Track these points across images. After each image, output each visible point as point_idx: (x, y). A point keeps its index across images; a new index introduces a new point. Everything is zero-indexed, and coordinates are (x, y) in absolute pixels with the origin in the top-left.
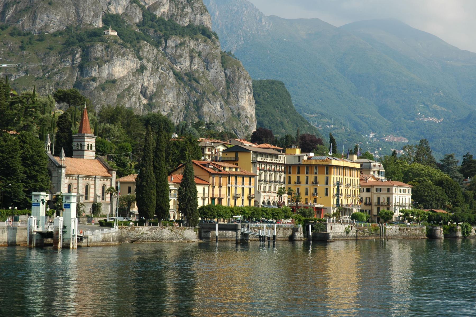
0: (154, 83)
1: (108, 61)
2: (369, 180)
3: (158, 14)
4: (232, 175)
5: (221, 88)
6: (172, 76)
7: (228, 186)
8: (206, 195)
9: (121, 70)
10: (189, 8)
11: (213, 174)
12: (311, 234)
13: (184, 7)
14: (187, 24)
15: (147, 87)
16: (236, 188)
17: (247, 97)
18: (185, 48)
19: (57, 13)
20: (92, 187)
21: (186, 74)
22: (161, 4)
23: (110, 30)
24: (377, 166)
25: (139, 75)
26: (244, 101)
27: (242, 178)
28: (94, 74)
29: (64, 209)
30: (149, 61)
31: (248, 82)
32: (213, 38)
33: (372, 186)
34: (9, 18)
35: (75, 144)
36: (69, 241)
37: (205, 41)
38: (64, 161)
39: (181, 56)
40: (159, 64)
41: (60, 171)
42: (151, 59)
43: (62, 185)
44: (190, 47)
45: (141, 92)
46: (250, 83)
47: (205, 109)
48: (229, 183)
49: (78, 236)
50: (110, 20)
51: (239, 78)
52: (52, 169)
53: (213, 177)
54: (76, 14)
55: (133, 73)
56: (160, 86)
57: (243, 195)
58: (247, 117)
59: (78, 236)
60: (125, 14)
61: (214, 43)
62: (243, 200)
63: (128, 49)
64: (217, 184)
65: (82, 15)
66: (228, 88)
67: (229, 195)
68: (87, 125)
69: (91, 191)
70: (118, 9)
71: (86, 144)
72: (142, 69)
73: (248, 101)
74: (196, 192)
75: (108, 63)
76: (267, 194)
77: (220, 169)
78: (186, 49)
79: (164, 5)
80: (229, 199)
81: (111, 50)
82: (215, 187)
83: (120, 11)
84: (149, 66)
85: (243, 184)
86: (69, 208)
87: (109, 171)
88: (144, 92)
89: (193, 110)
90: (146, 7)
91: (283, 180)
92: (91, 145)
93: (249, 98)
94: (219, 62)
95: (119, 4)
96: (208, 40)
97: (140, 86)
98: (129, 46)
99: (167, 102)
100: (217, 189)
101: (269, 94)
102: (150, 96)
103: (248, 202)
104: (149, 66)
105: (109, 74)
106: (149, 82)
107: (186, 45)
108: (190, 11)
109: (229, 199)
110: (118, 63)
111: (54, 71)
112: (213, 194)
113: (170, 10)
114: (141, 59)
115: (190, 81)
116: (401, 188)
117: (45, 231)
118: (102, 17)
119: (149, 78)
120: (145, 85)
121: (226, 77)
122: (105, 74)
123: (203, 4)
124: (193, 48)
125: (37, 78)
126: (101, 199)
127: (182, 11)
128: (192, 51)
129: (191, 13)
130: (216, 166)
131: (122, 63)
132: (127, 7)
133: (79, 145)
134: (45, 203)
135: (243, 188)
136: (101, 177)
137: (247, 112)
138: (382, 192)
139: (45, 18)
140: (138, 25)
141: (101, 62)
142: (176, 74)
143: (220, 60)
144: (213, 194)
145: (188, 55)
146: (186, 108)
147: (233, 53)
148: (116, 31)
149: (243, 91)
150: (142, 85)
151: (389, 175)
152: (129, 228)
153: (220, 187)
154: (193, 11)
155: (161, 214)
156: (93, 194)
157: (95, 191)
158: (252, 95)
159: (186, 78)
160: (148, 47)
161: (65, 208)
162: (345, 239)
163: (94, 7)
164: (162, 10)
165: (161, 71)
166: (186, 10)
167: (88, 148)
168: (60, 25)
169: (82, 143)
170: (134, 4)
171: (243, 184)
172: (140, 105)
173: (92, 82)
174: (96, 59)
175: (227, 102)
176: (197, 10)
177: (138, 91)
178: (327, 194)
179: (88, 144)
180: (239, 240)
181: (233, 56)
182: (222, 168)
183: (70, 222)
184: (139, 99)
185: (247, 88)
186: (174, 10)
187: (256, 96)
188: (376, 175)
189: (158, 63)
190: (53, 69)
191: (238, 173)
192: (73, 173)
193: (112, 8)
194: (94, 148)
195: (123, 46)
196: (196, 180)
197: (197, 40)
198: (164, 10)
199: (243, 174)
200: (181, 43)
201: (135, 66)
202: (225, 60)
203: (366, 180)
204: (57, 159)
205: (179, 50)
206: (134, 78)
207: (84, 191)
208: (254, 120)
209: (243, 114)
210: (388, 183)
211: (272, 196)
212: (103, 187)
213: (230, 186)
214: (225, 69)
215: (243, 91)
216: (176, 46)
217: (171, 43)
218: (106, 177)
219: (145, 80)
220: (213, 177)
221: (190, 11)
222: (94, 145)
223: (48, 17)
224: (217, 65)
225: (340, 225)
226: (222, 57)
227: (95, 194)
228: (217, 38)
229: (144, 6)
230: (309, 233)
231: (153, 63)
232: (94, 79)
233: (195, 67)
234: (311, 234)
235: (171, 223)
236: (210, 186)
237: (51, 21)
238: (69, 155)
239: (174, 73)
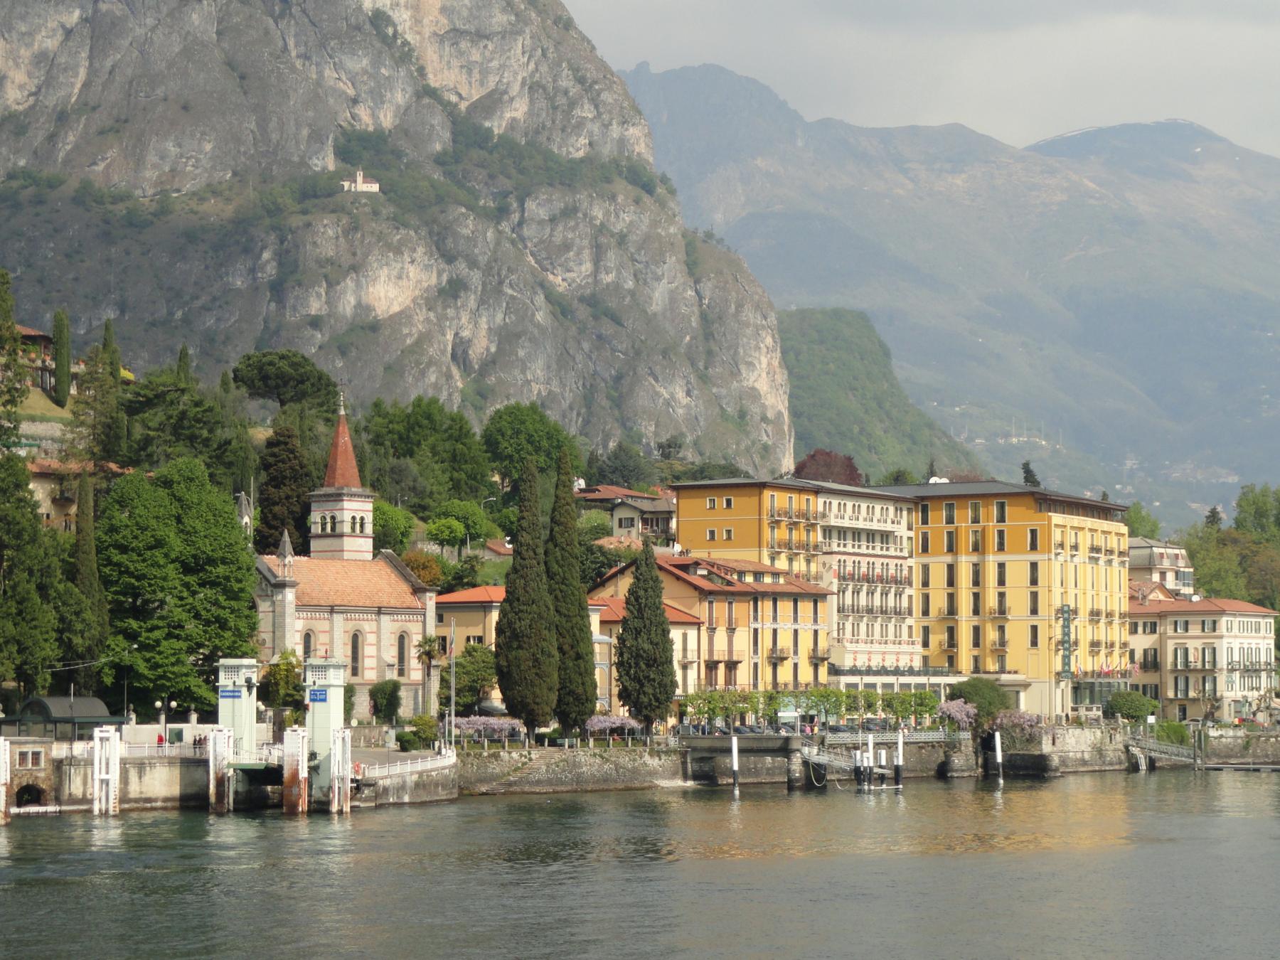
0: (490, 328)
1: (355, 268)
2: (1151, 597)
3: (496, 126)
4: (764, 595)
5: (688, 338)
6: (543, 305)
7: (753, 626)
8: (692, 656)
9: (392, 292)
10: (586, 107)
11: (711, 593)
12: (999, 759)
13: (572, 104)
14: (581, 154)
15: (470, 341)
16: (775, 631)
17: (764, 360)
18: (577, 224)
19: (203, 133)
20: (371, 638)
21: (582, 299)
22: (506, 97)
23: (360, 179)
24: (1172, 557)
25: (445, 308)
26: (756, 373)
27: (812, 604)
28: (315, 306)
29: (311, 705)
30: (473, 264)
31: (766, 318)
32: (660, 190)
33: (1162, 616)
34: (67, 155)
35: (315, 517)
36: (327, 795)
37: (637, 202)
38: (286, 565)
39: (567, 247)
40: (504, 273)
42: (480, 258)
43: (288, 635)
44: (593, 218)
45: (454, 357)
46: (772, 319)
47: (641, 399)
48: (756, 619)
49: (352, 781)
50: (360, 149)
51: (740, 306)
53: (711, 603)
54: (259, 137)
55: (427, 299)
56: (507, 337)
57: (796, 652)
58: (764, 419)
59: (352, 781)
60: (402, 129)
61: (662, 204)
62: (796, 665)
63: (412, 233)
64: (721, 622)
65: (275, 137)
66: (708, 336)
67: (756, 652)
68: (346, 465)
69: (368, 651)
70: (382, 116)
71: (347, 516)
72: (452, 291)
73: (768, 373)
74: (671, 642)
75: (354, 275)
76: (862, 647)
77: (728, 577)
78: (581, 225)
79: (512, 99)
80: (756, 665)
81: (363, 236)
82: (717, 632)
83: (387, 120)
84: (475, 278)
85: (796, 620)
87: (417, 591)
88: (460, 355)
89: (605, 403)
90: (463, 106)
91: (905, 604)
92: (362, 519)
93: (769, 364)
94: (678, 261)
95: (383, 103)
96: (646, 199)
97: (450, 337)
98: (414, 221)
99: (528, 382)
100: (721, 636)
101: (829, 350)
102: (480, 367)
103: (811, 670)
104: (475, 278)
105: (359, 305)
106: (477, 329)
107: (580, 215)
108: (590, 116)
109: (756, 665)
110: (384, 272)
111: (198, 303)
112: (711, 651)
113: (531, 113)
114: (450, 259)
115: (596, 318)
116: (1246, 620)
117: (261, 764)
118: (336, 140)
119: (475, 314)
120: (466, 334)
121: (701, 305)
122: (347, 304)
123: (626, 94)
124: (602, 224)
125: (153, 324)
126: (396, 672)
127: (568, 113)
128: (600, 231)
129: (592, 120)
130: (715, 570)
131: (395, 273)
132: (408, 108)
133: (358, 520)
134: (254, 691)
135: (796, 631)
136: (393, 611)
137: (764, 406)
138: (1191, 633)
139: (172, 149)
140: (440, 160)
141: (335, 273)
142: (551, 297)
143: (682, 256)
144: (711, 651)
145: (586, 242)
146: (585, 397)
147: (718, 233)
148: (378, 180)
149: (753, 343)
150: (456, 334)
151: (1208, 583)
153: (731, 630)
154: (599, 114)
155: (573, 712)
156: (374, 660)
157: (379, 650)
158: (779, 354)
159: (583, 312)
160: (470, 222)
161: (313, 700)
162: (1096, 768)
163: (311, 114)
164: (508, 115)
165: (510, 292)
166: (577, 112)
167: (353, 529)
168: (213, 167)
169: (337, 514)
170: (426, 100)
171: (796, 620)
172: (450, 395)
173: (309, 332)
174: (323, 262)
175: (704, 379)
176: (610, 112)
177: (443, 352)
178: (1034, 643)
179: (354, 518)
180: (797, 780)
181: (720, 241)
182: (735, 577)
183: (326, 739)
184: (449, 376)
185: (763, 333)
186: (544, 115)
187: (791, 358)
188: (1171, 583)
189: (500, 270)
190: (197, 298)
191: (779, 589)
192: (315, 602)
193: (363, 113)
194: (369, 529)
195: (398, 222)
196: (670, 615)
197: (613, 198)
198: (514, 114)
199: (796, 590)
200: (566, 208)
201: (434, 281)
202: (697, 254)
203: (1144, 597)
204: (270, 560)
205: (560, 228)
206: (432, 315)
207: (349, 653)
208: (786, 428)
209: (755, 410)
210: (1208, 606)
211: (877, 653)
212: (401, 640)
213: (758, 626)
214: (697, 282)
215: (753, 343)
216: (553, 220)
217: (536, 208)
218: (409, 610)
219: (464, 320)
220: (711, 603)
221: (590, 116)
222: (369, 518)
223: (180, 146)
224: (673, 264)
225: (1078, 731)
226: (687, 245)
227: (379, 658)
228: (672, 192)
229: (456, 105)
230: (995, 757)
231: (488, 271)
232: (315, 322)
233: (608, 278)
234: (999, 759)
235: (601, 736)
236: (703, 628)
237: (188, 158)
238: (302, 549)
239: (548, 298)
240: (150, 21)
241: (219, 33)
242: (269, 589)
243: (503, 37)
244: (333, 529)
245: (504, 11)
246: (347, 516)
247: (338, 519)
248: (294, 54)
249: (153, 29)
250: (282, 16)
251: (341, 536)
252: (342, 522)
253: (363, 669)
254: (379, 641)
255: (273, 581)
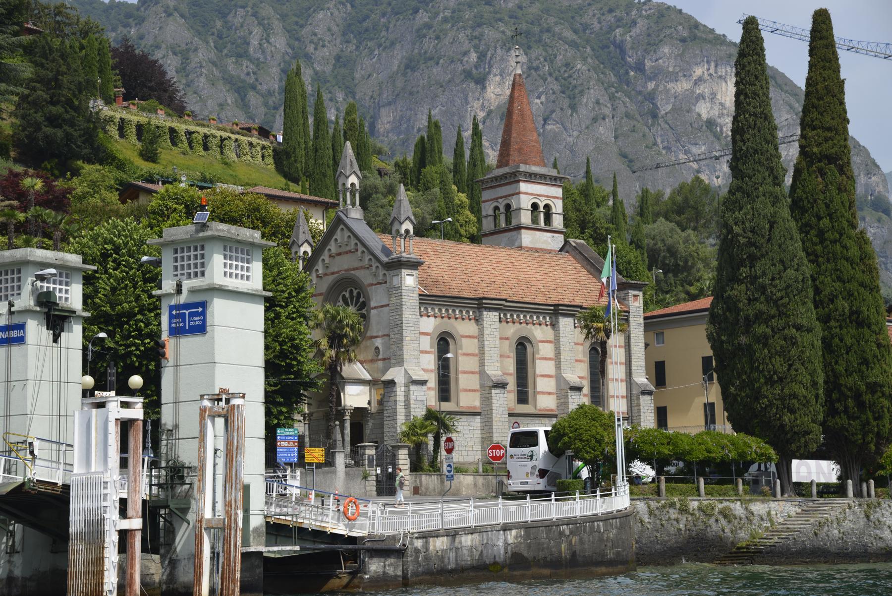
20: (546, 350)
29: (170, 345)
37: (879, 221)
41: (395, 281)
43: (407, 338)
52: (365, 277)
69: (542, 367)
71: (526, 202)
86: (200, 329)
133: (502, 210)
152: (573, 446)
157: (558, 367)
161: (176, 332)
167: (535, 220)
192: (455, 294)
194: (558, 222)
222: (558, 207)
227: (559, 378)
240: (575, 133)
241: (616, 137)
242: (381, 272)
243: (789, 128)
244: (508, 221)
245: (788, 113)
246: (526, 202)
247: (514, 206)
248: (661, 146)
249: (578, 137)
250: (653, 125)
251: (519, 228)
252: (519, 209)
253: (535, 393)
254: (558, 353)
255: (385, 259)
